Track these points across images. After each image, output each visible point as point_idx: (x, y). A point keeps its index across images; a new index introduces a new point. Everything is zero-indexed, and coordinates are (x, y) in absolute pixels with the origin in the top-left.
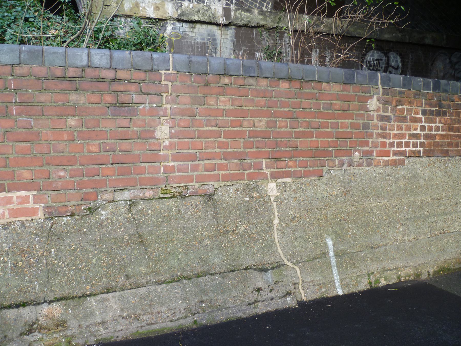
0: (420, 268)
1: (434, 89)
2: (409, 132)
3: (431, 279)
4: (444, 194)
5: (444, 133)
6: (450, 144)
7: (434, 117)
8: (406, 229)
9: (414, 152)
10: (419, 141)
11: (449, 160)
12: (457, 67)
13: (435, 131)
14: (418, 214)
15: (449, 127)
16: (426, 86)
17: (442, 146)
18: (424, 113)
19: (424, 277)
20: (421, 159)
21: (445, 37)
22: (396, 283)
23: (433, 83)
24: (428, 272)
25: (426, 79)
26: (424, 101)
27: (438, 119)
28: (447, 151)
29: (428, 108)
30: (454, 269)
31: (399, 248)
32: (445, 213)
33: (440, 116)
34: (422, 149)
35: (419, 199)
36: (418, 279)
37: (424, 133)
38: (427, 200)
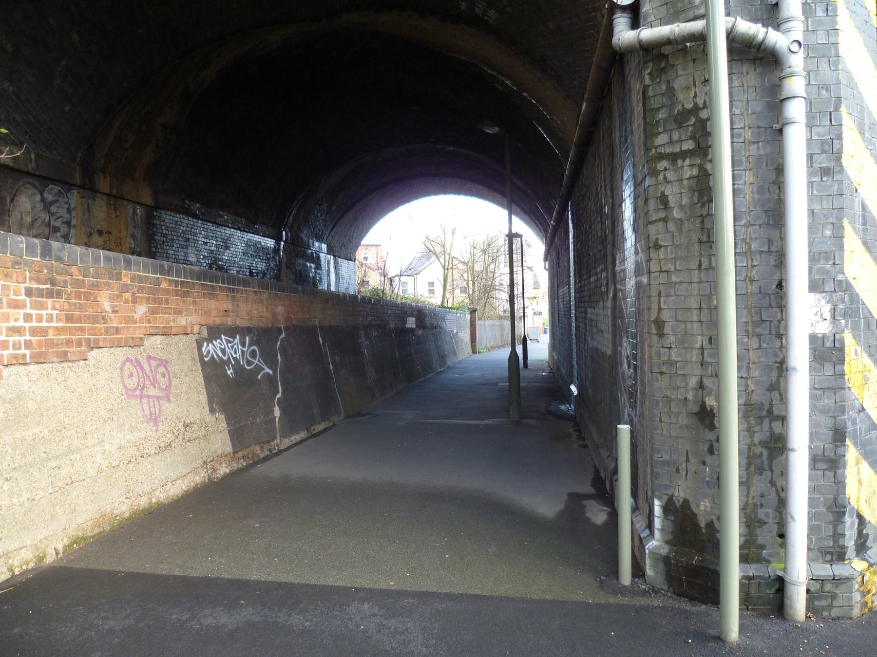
0: (43, 546)
1: (43, 255)
2: (7, 325)
3: (61, 559)
4: (66, 421)
5: (60, 325)
6: (69, 343)
7: (44, 299)
8: (14, 485)
9: (16, 357)
10: (22, 339)
11: (69, 367)
12: (53, 209)
13: (47, 321)
14: (30, 459)
15: (67, 316)
16: (31, 250)
17: (57, 345)
18: (29, 292)
19: (50, 559)
20: (26, 367)
21: (33, 156)
22: (7, 580)
23: (41, 246)
24: (55, 549)
25: (30, 239)
26: (28, 273)
27: (50, 301)
28: (66, 353)
29: (35, 286)
30: (92, 537)
31: (5, 520)
32: (70, 451)
33: (53, 297)
34: (28, 352)
35: (29, 433)
36: (42, 564)
37: (31, 325)
38: (43, 434)
